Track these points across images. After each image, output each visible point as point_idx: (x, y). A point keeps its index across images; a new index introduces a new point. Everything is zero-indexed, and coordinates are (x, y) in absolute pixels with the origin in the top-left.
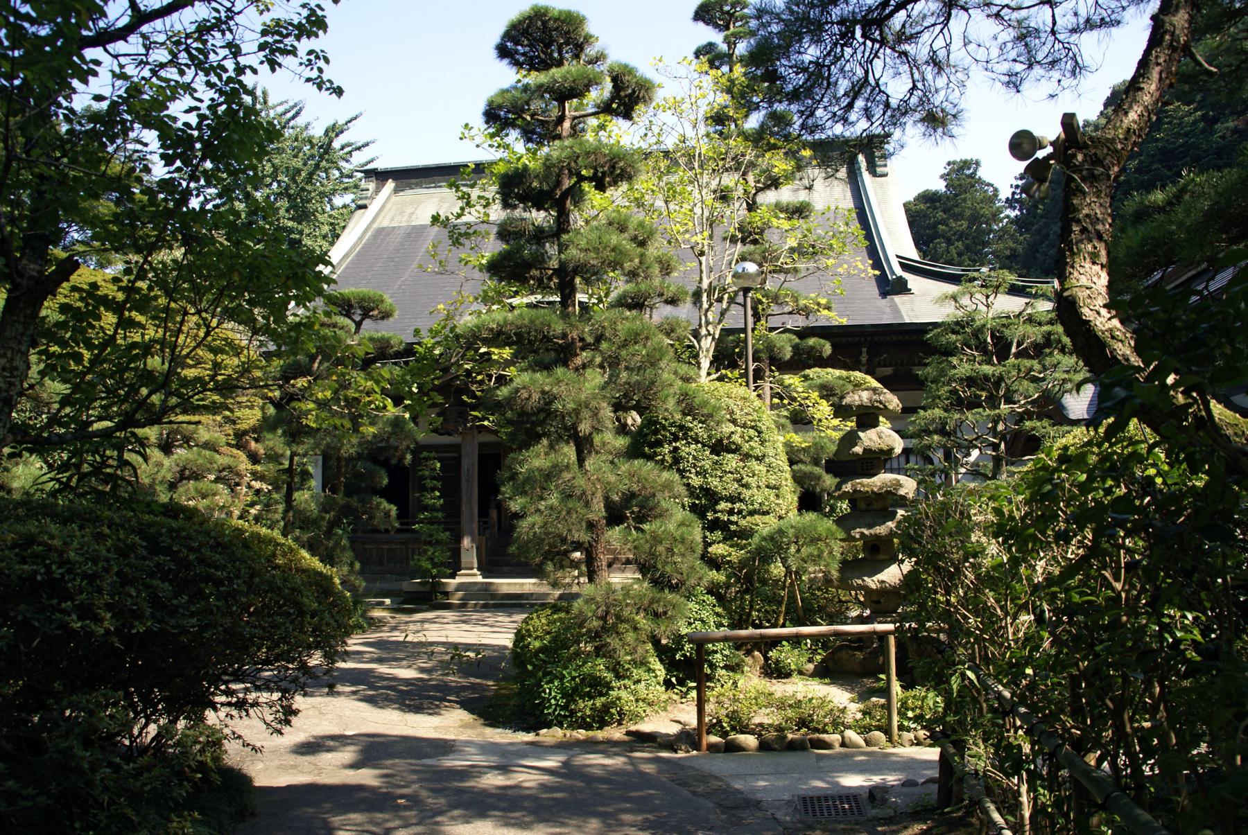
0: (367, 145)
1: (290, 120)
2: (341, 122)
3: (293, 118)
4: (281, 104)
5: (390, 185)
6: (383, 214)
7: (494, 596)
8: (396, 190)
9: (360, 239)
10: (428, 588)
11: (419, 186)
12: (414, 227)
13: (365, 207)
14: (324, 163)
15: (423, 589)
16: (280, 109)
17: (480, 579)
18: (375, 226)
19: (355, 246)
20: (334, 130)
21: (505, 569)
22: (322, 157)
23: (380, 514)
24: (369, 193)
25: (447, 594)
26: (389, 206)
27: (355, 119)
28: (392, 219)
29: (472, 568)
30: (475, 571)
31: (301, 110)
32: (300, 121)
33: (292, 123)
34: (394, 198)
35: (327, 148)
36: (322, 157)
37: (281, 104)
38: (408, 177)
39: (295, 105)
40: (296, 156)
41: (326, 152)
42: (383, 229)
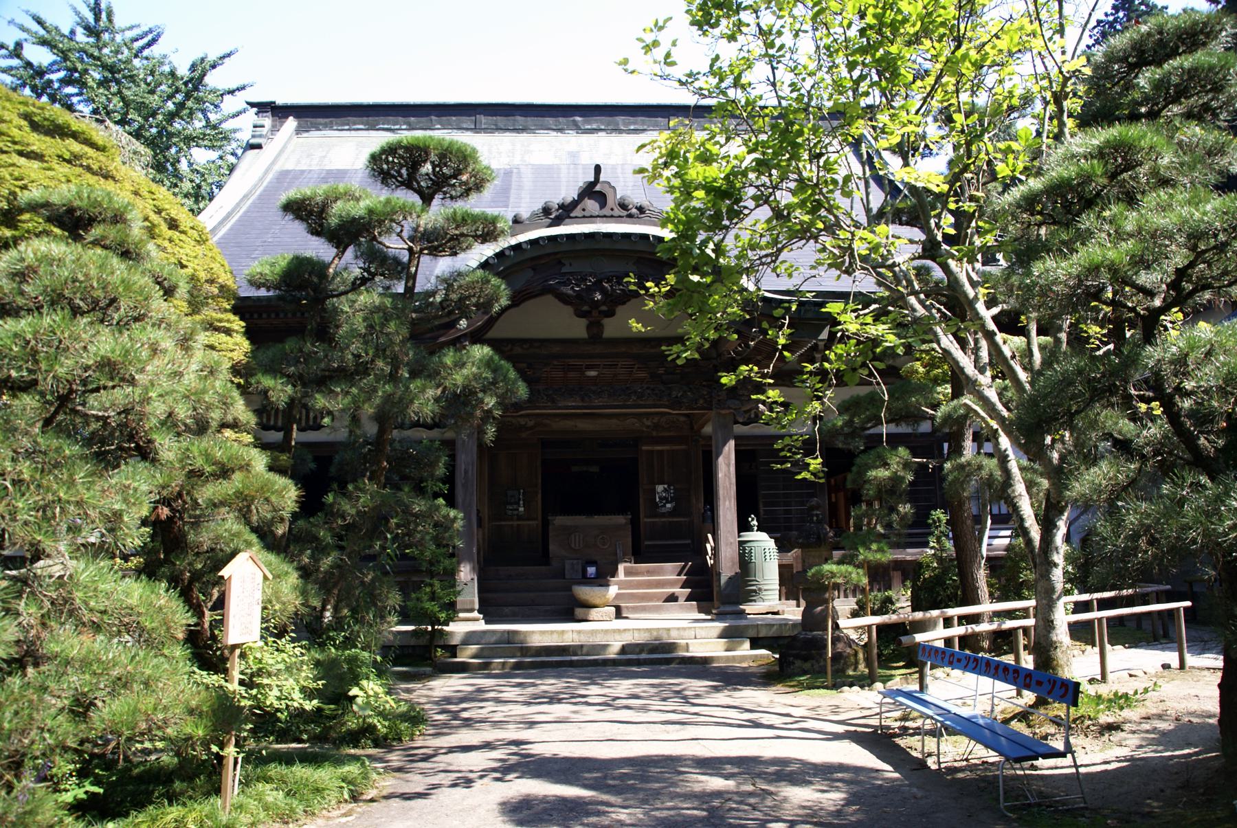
0: (243, 88)
1: (143, 48)
2: (212, 57)
3: (149, 44)
4: (131, 28)
5: (291, 123)
6: (284, 156)
7: (526, 651)
8: (299, 131)
9: (262, 179)
10: (423, 641)
11: (326, 126)
12: (329, 172)
13: (259, 147)
14: (189, 104)
15: (413, 642)
16: (130, 35)
17: (481, 626)
18: (277, 168)
19: (255, 186)
20: (200, 69)
21: (507, 610)
22: (188, 96)
23: (425, 529)
24: (264, 131)
25: (453, 650)
26: (290, 148)
27: (229, 55)
28: (299, 162)
29: (472, 610)
30: (475, 614)
31: (159, 35)
32: (156, 51)
33: (146, 53)
34: (296, 140)
35: (196, 81)
36: (188, 96)
37: (131, 28)
38: (314, 115)
39: (151, 31)
40: (152, 92)
41: (196, 89)
42: (287, 172)
